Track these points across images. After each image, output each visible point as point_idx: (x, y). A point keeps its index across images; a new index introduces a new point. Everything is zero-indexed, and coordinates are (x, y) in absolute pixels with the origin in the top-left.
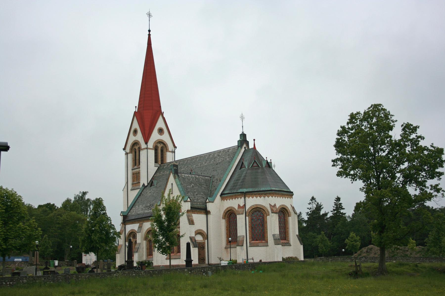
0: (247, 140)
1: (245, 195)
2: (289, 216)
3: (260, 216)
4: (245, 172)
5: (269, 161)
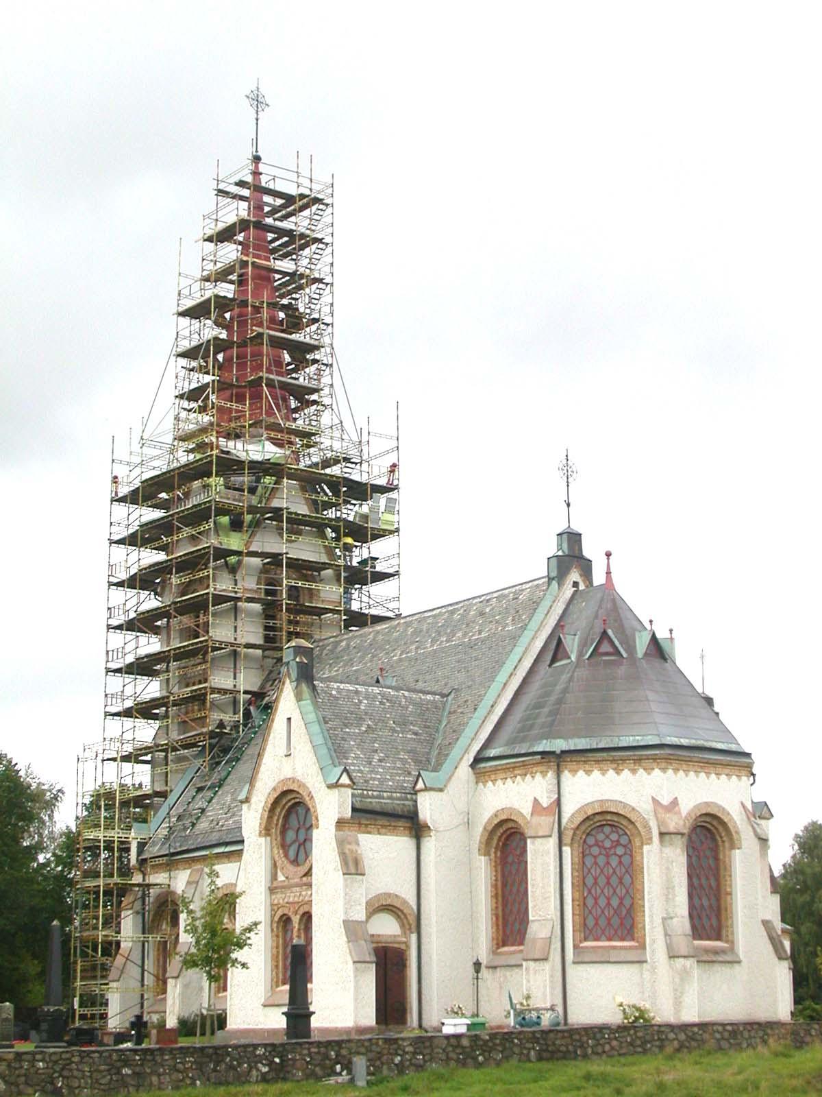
1: (558, 761)
2: (733, 847)
3: (618, 843)
4: (565, 677)
5: (661, 635)
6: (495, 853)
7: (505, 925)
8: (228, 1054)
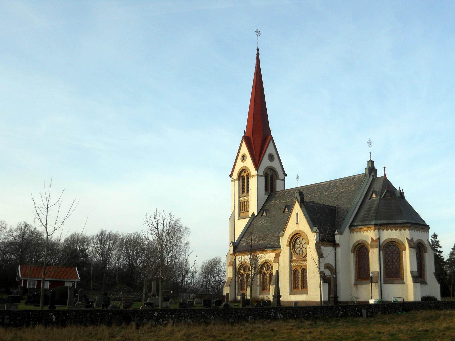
7: (359, 273)
8: (333, 308)
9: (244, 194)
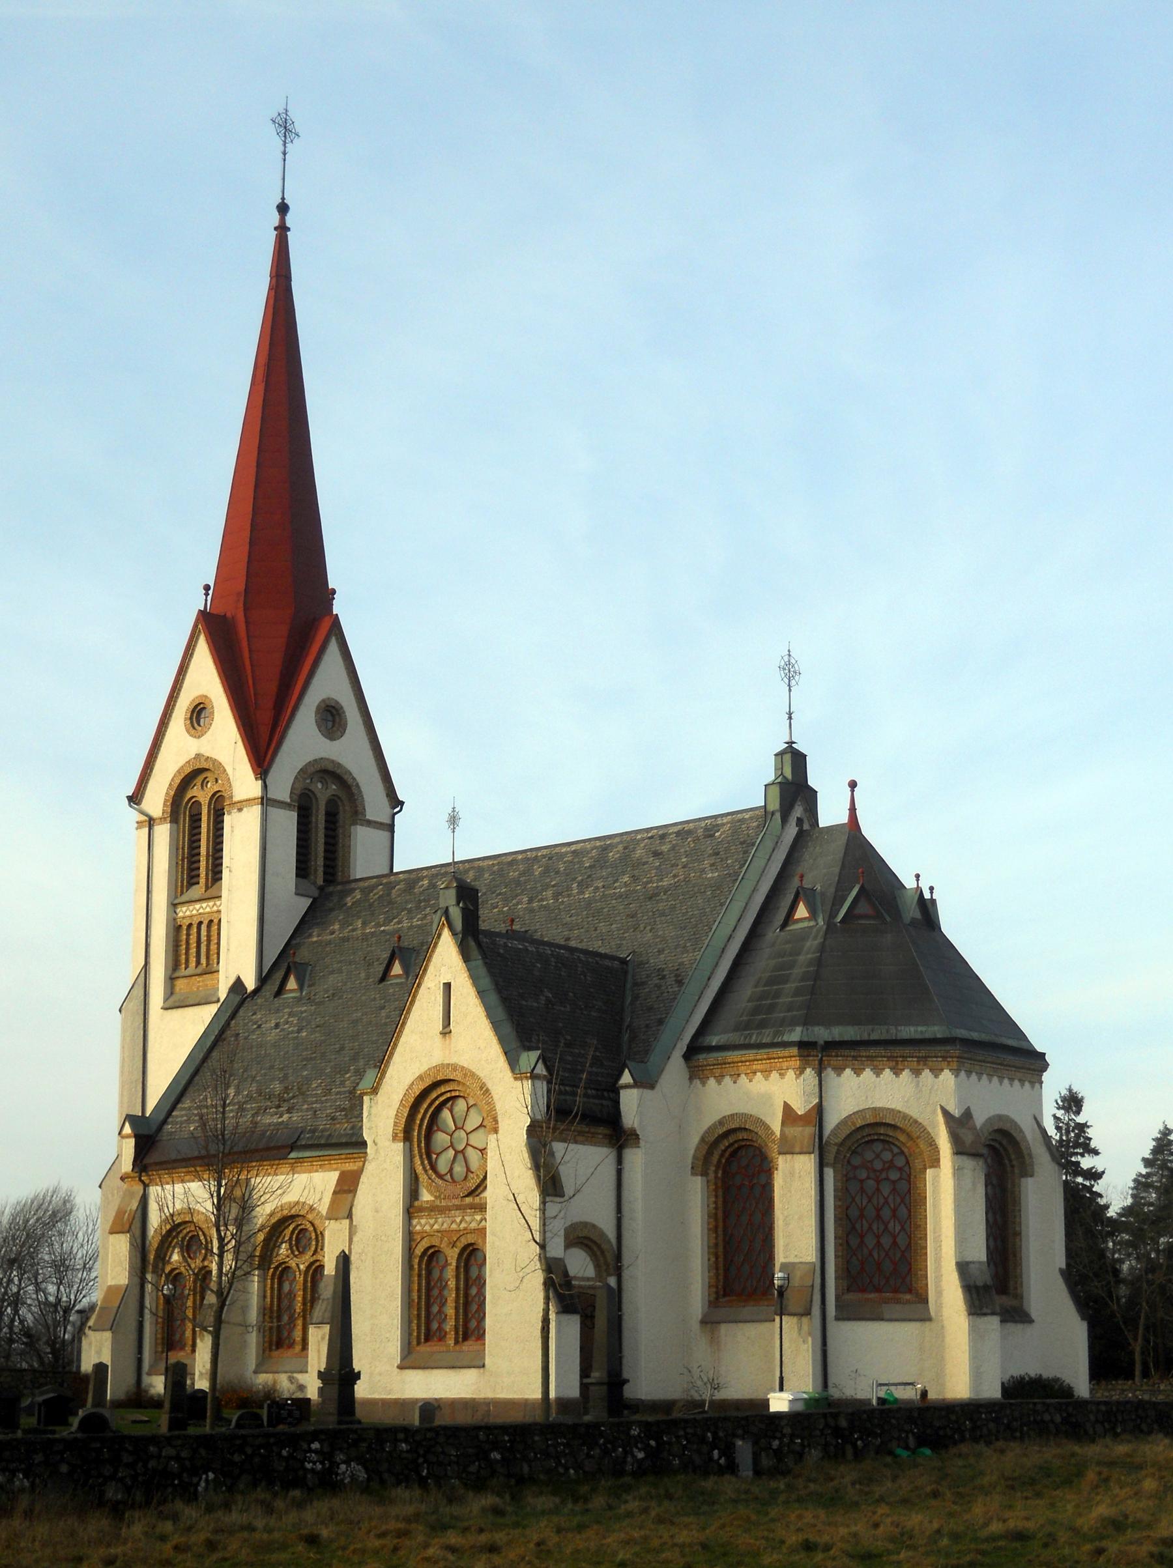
0: (811, 782)
5: (927, 895)
6: (716, 1172)
9: (198, 890)
